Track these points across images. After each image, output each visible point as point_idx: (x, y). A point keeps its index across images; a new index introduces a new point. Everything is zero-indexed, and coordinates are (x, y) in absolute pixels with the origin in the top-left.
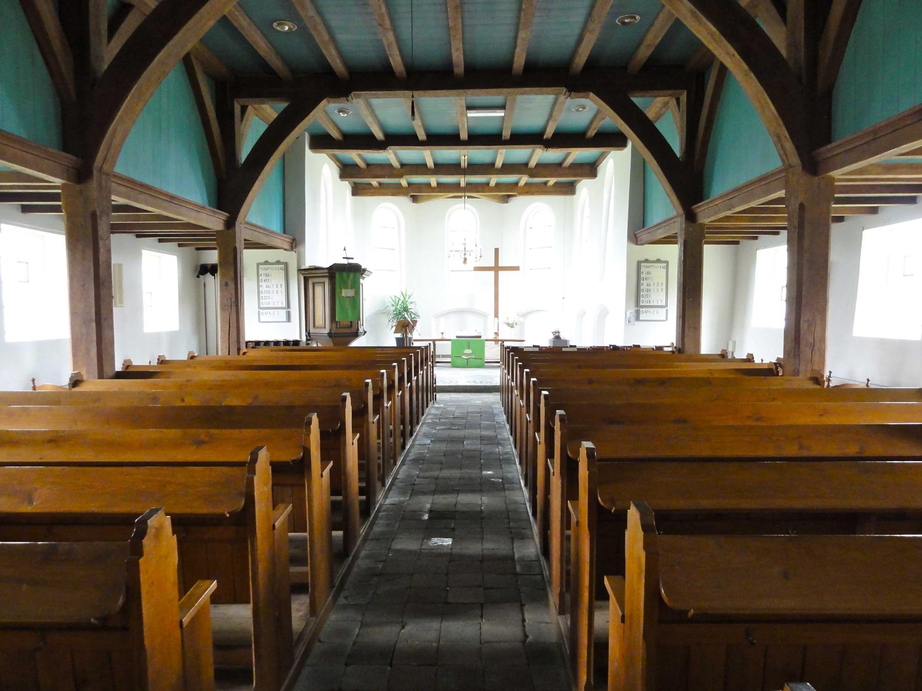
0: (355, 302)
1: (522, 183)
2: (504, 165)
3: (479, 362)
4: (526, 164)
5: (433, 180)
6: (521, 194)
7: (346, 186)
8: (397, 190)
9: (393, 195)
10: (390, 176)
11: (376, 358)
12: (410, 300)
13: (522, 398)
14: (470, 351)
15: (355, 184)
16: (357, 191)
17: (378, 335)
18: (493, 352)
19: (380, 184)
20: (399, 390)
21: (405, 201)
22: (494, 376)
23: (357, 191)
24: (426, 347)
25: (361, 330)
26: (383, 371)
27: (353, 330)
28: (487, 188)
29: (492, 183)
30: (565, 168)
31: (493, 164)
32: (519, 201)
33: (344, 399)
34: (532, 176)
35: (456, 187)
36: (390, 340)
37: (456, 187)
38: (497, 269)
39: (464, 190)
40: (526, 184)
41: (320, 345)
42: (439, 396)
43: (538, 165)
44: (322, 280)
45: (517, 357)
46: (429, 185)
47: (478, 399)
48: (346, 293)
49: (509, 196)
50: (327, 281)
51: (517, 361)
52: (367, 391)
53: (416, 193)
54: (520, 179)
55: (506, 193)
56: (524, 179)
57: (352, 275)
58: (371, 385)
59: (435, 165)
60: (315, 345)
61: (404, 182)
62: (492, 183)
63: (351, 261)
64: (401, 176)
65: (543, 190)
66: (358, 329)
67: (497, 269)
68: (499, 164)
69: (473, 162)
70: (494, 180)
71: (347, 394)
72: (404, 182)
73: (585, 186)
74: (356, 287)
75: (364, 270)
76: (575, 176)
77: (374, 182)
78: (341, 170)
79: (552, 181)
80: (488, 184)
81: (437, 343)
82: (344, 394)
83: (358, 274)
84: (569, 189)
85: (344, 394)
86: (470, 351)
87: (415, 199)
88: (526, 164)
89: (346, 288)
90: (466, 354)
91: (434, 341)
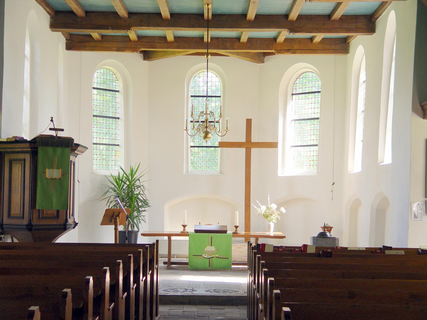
0: (64, 185)
1: (281, 39)
2: (258, 16)
3: (224, 262)
4: (286, 16)
5: (170, 34)
6: (280, 51)
7: (59, 38)
8: (124, 45)
9: (118, 50)
10: (115, 27)
11: (92, 256)
12: (137, 183)
13: (266, 316)
14: (213, 249)
15: (71, 35)
16: (71, 45)
17: (87, 229)
18: (240, 251)
19: (103, 36)
20: (111, 301)
21: (135, 58)
22: (240, 282)
23: (71, 45)
24: (152, 246)
25: (70, 221)
26: (69, 290)
27: (61, 221)
28: (237, 44)
29: (244, 39)
30: (334, 21)
31: (245, 15)
32: (276, 61)
33: (105, 271)
34: (292, 30)
35: (198, 42)
36: (107, 236)
37: (198, 42)
38: (248, 145)
39: (207, 46)
40: (286, 40)
41: (15, 240)
42: (163, 309)
43: (300, 17)
44: (22, 156)
45: (267, 259)
46: (164, 38)
47: (220, 314)
48: (53, 173)
49: (265, 54)
50: (28, 157)
51: (264, 266)
52: (65, 303)
53: (149, 50)
54: (280, 33)
55: (261, 50)
56: (284, 34)
57: (59, 150)
58: (70, 295)
59: (172, 15)
60: (9, 241)
61: (132, 35)
62: (244, 39)
63: (60, 134)
64: (128, 28)
65: (307, 47)
66: (66, 220)
67: (248, 145)
68: (251, 16)
69: (219, 12)
70: (246, 34)
71: (69, 290)
72: (132, 35)
73: (360, 45)
74: (67, 170)
75: (77, 145)
76: (348, 31)
77: (95, 34)
78: (52, 18)
79: (319, 37)
80: (239, 39)
81: (173, 238)
82: (32, 308)
83: (67, 150)
84: (342, 46)
85: (32, 308)
86: (213, 249)
87: (147, 56)
88: (286, 16)
89: (52, 167)
90: (208, 252)
91: (170, 236)
